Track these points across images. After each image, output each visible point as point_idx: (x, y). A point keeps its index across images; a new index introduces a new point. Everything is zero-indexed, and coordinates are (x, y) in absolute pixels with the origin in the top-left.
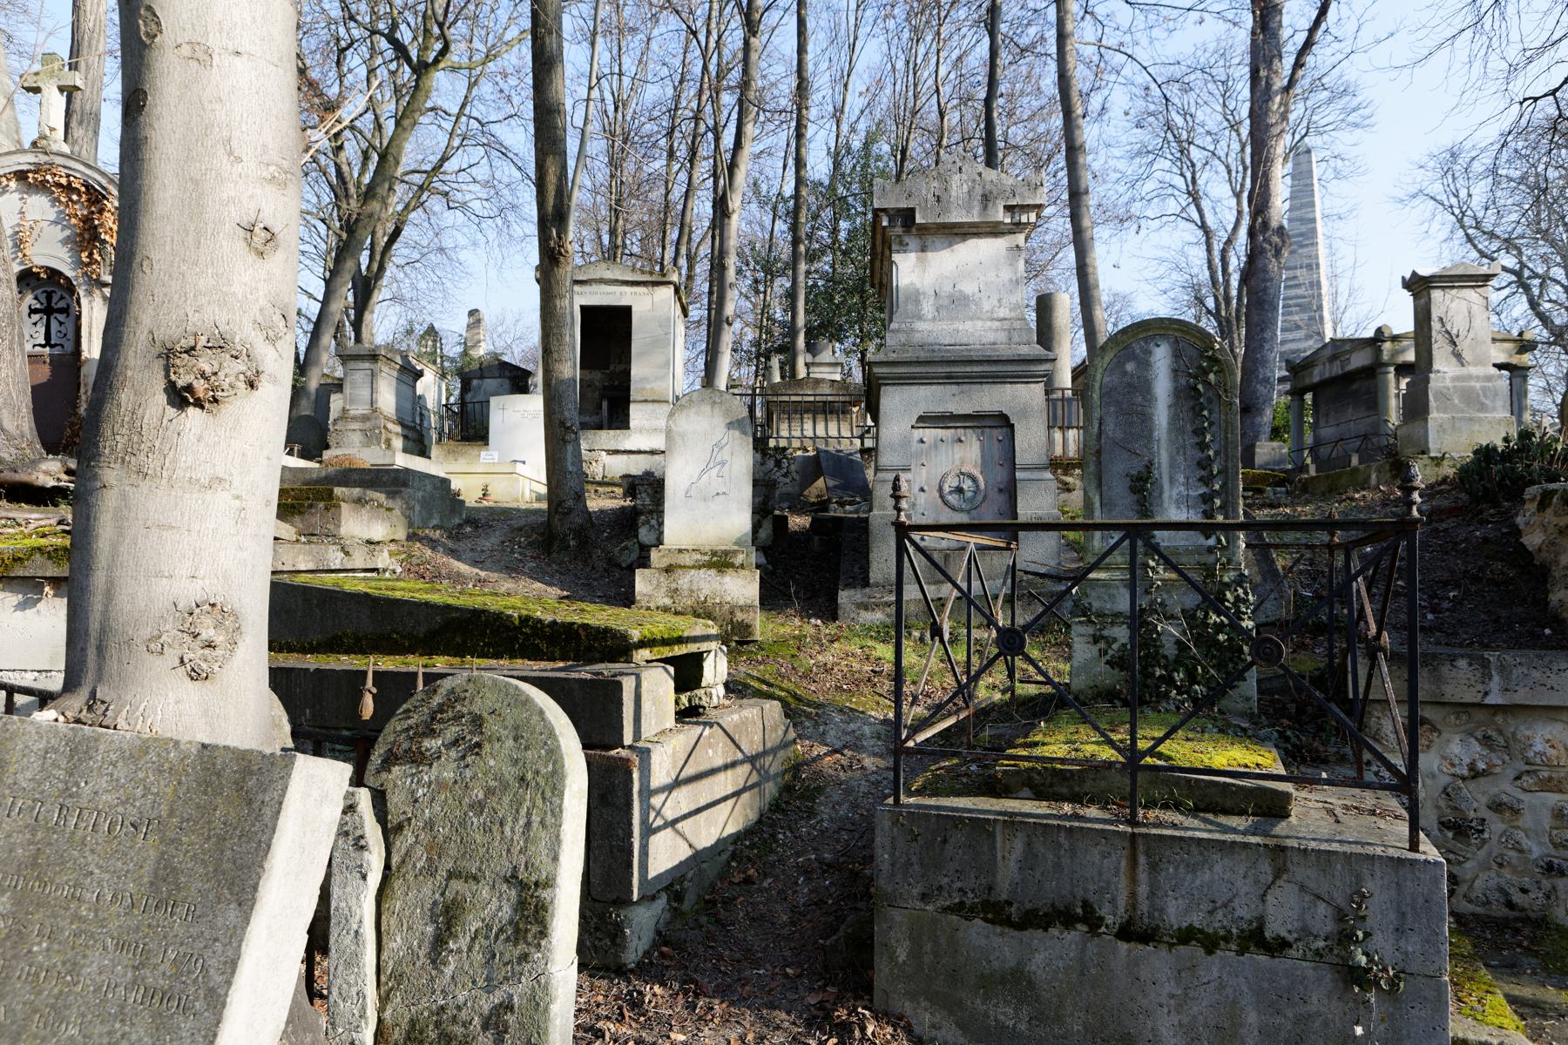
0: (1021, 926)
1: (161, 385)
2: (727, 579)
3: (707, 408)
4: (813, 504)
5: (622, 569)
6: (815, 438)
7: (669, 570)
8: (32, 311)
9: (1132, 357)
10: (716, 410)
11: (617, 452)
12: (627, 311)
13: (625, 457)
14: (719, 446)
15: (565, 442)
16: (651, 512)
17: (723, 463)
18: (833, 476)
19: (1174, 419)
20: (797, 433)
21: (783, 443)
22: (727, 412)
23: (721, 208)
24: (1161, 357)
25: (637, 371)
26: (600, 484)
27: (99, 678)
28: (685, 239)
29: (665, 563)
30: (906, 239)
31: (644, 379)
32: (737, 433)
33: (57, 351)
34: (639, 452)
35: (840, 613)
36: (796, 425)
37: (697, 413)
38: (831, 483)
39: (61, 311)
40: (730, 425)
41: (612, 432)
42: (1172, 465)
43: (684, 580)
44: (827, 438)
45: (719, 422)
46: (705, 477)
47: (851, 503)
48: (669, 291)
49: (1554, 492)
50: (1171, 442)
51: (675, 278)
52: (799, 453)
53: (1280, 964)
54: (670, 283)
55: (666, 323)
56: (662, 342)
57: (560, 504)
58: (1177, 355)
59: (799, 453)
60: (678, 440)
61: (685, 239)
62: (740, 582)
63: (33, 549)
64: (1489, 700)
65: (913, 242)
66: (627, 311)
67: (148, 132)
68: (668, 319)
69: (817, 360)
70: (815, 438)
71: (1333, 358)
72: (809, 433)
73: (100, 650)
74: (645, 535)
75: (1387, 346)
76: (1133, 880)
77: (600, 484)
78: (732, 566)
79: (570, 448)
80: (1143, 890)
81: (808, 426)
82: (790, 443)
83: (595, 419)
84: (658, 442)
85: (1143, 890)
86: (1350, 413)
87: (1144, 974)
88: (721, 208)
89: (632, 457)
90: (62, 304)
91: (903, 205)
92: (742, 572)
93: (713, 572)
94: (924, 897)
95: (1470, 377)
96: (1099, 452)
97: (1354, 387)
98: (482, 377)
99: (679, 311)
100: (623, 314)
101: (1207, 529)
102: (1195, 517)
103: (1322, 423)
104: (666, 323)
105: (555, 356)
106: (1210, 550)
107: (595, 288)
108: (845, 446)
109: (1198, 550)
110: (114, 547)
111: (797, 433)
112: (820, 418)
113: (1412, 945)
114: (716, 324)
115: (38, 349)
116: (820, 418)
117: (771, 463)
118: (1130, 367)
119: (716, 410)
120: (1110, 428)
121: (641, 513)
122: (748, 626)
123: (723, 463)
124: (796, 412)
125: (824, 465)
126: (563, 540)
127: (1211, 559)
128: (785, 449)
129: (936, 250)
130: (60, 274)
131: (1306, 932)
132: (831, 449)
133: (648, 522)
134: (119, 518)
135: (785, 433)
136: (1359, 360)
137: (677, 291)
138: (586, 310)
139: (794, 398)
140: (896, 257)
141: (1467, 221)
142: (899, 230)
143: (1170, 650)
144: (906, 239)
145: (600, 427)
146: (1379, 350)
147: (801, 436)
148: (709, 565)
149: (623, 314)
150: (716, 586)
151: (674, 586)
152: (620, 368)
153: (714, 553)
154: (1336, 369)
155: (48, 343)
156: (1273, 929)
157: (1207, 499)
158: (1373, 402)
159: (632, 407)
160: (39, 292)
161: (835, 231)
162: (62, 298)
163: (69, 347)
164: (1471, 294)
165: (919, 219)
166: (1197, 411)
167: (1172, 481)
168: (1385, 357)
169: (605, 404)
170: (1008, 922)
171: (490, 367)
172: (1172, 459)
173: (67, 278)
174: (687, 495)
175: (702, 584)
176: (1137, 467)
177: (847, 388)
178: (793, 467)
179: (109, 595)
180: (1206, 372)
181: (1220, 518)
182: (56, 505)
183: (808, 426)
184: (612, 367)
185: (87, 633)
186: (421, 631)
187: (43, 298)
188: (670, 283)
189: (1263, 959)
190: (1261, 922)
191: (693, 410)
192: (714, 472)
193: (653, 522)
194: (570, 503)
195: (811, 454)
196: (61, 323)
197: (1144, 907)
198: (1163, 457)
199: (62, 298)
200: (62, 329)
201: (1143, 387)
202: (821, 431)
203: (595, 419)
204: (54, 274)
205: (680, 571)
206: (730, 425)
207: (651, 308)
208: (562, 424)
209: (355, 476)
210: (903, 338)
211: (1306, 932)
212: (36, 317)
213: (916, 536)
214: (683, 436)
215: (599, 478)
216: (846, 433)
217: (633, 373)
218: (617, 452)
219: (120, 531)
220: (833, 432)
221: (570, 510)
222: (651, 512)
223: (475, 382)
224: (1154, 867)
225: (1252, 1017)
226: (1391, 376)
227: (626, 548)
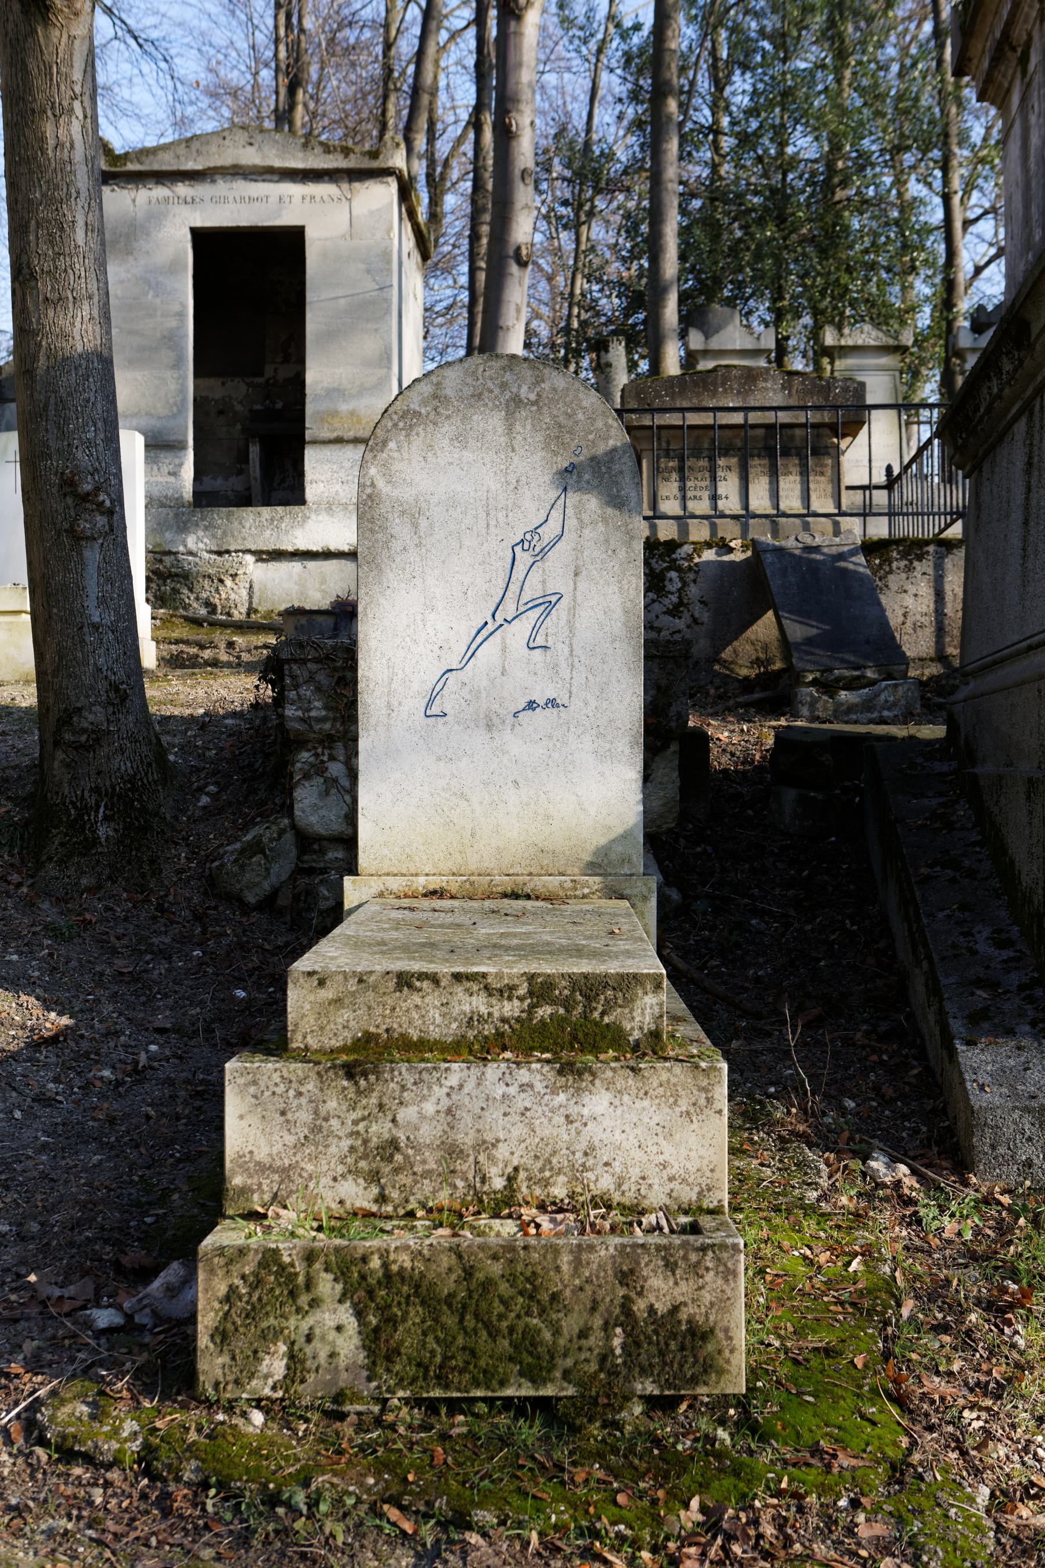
2: (597, 1102)
3: (491, 422)
4: (747, 685)
5: (245, 908)
6: (744, 518)
7: (362, 1061)
10: (524, 427)
11: (277, 555)
12: (292, 240)
13: (295, 567)
14: (533, 546)
15: (78, 538)
16: (328, 740)
17: (548, 604)
18: (802, 613)
20: (701, 506)
22: (557, 436)
23: (495, 70)
25: (317, 375)
26: (240, 627)
28: (423, 123)
29: (343, 1027)
31: (336, 392)
32: (592, 503)
34: (327, 555)
35: (982, 1142)
36: (698, 485)
37: (460, 440)
38: (797, 631)
40: (569, 478)
41: (266, 512)
43: (424, 1106)
44: (775, 518)
45: (533, 469)
46: (489, 651)
47: (851, 685)
48: (390, 190)
51: (398, 160)
52: (709, 555)
54: (388, 172)
55: (380, 263)
56: (375, 308)
57: (66, 719)
59: (709, 555)
60: (400, 528)
61: (423, 123)
62: (650, 1112)
66: (292, 240)
68: (385, 256)
69: (715, 344)
70: (744, 518)
72: (730, 504)
74: (309, 805)
77: (240, 627)
78: (613, 1038)
79: (92, 555)
81: (729, 487)
82: (684, 530)
83: (236, 483)
84: (341, 533)
88: (495, 70)
89: (312, 565)
92: (662, 1074)
93: (537, 1074)
99: (409, 243)
100: (286, 246)
104: (380, 263)
105: (45, 286)
107: (222, 187)
108: (821, 535)
111: (701, 506)
112: (758, 467)
114: (494, 259)
116: (758, 467)
119: (524, 427)
121: (301, 743)
122: (699, 1335)
123: (548, 604)
124: (697, 454)
125: (775, 584)
128: (672, 546)
132: (790, 543)
133: (320, 769)
135: (670, 506)
137: (405, 192)
138: (201, 237)
139: (694, 419)
145: (246, 501)
147: (733, 505)
148: (518, 1041)
149: (286, 246)
150: (552, 1129)
151: (380, 1130)
152: (285, 372)
153: (541, 990)
159: (312, 457)
161: (718, 103)
169: (255, 451)
174: (432, 710)
175: (496, 1124)
177: (827, 390)
178: (693, 591)
183: (729, 487)
184: (269, 371)
188: (388, 172)
191: (447, 429)
192: (521, 629)
193: (336, 769)
194: (96, 716)
195: (738, 556)
202: (760, 500)
203: (236, 483)
205: (405, 1073)
206: (569, 478)
207: (348, 226)
208: (69, 485)
214: (413, 514)
215: (239, 614)
216: (822, 503)
217: (310, 377)
218: (277, 555)
220: (790, 501)
221: (98, 737)
222: (328, 740)
227: (257, 847)
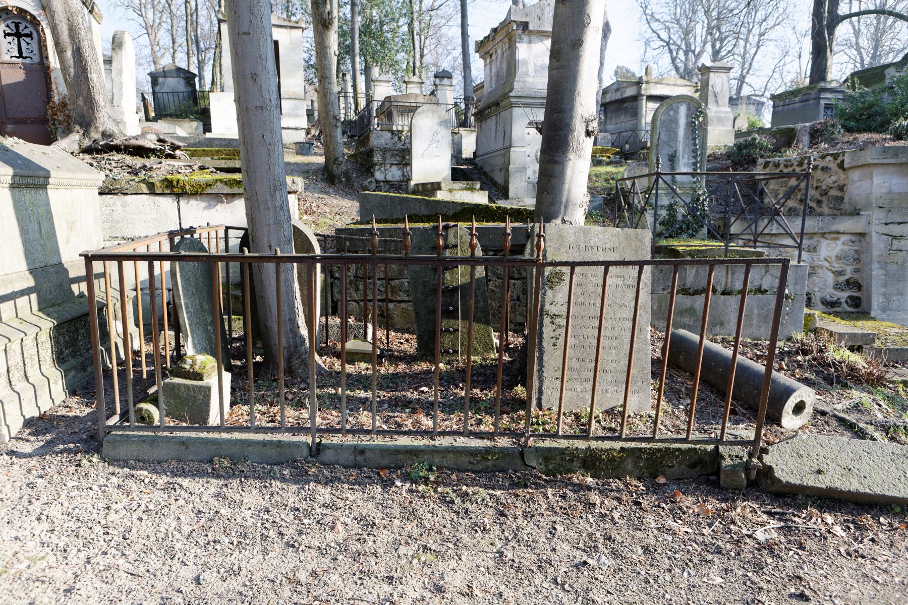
0: (693, 295)
1: (584, 130)
8: (6, 35)
9: (673, 109)
14: (436, 133)
16: (381, 164)
17: (438, 141)
19: (686, 134)
21: (400, 128)
24: (683, 110)
27: (565, 214)
30: (523, 36)
33: (28, 61)
39: (27, 35)
42: (684, 151)
49: (770, 162)
50: (684, 142)
53: (764, 296)
58: (689, 109)
63: (217, 180)
64: (773, 232)
65: (525, 38)
67: (582, 53)
71: (617, 90)
73: (566, 207)
75: (644, 86)
76: (727, 278)
80: (729, 280)
85: (729, 280)
86: (623, 118)
87: (728, 304)
90: (26, 31)
91: (524, 20)
93: (469, 192)
94: (663, 289)
95: (720, 112)
96: (658, 146)
97: (625, 105)
98: (165, 76)
101: (693, 175)
102: (690, 171)
103: (608, 122)
106: (694, 182)
109: (690, 182)
110: (571, 179)
113: (798, 288)
115: (14, 59)
117: (396, 139)
118: (671, 113)
120: (663, 136)
123: (438, 141)
126: (339, 178)
127: (694, 186)
129: (535, 43)
130: (26, 12)
131: (772, 287)
134: (573, 169)
136: (630, 92)
140: (518, 45)
141: (648, 12)
142: (520, 32)
143: (680, 218)
144: (523, 36)
146: (640, 87)
154: (618, 96)
155: (21, 55)
156: (764, 287)
157: (695, 164)
158: (635, 114)
160: (9, 22)
162: (26, 27)
163: (36, 59)
164: (724, 76)
165: (531, 27)
166: (693, 131)
167: (683, 157)
168: (643, 92)
170: (690, 294)
171: (170, 71)
172: (684, 149)
173: (31, 15)
176: (671, 151)
179: (569, 191)
180: (698, 117)
181: (699, 171)
182: (149, 157)
185: (561, 202)
186: (451, 213)
187: (13, 26)
189: (760, 296)
190: (761, 286)
196: (28, 44)
197: (729, 285)
198: (681, 148)
199: (26, 27)
200: (29, 47)
201: (675, 121)
204: (22, 12)
209: (217, 142)
210: (521, 85)
211: (772, 287)
212: (9, 39)
213: (663, 176)
219: (573, 173)
222: (381, 164)
223: (161, 80)
224: (733, 274)
225: (756, 311)
226: (644, 101)
